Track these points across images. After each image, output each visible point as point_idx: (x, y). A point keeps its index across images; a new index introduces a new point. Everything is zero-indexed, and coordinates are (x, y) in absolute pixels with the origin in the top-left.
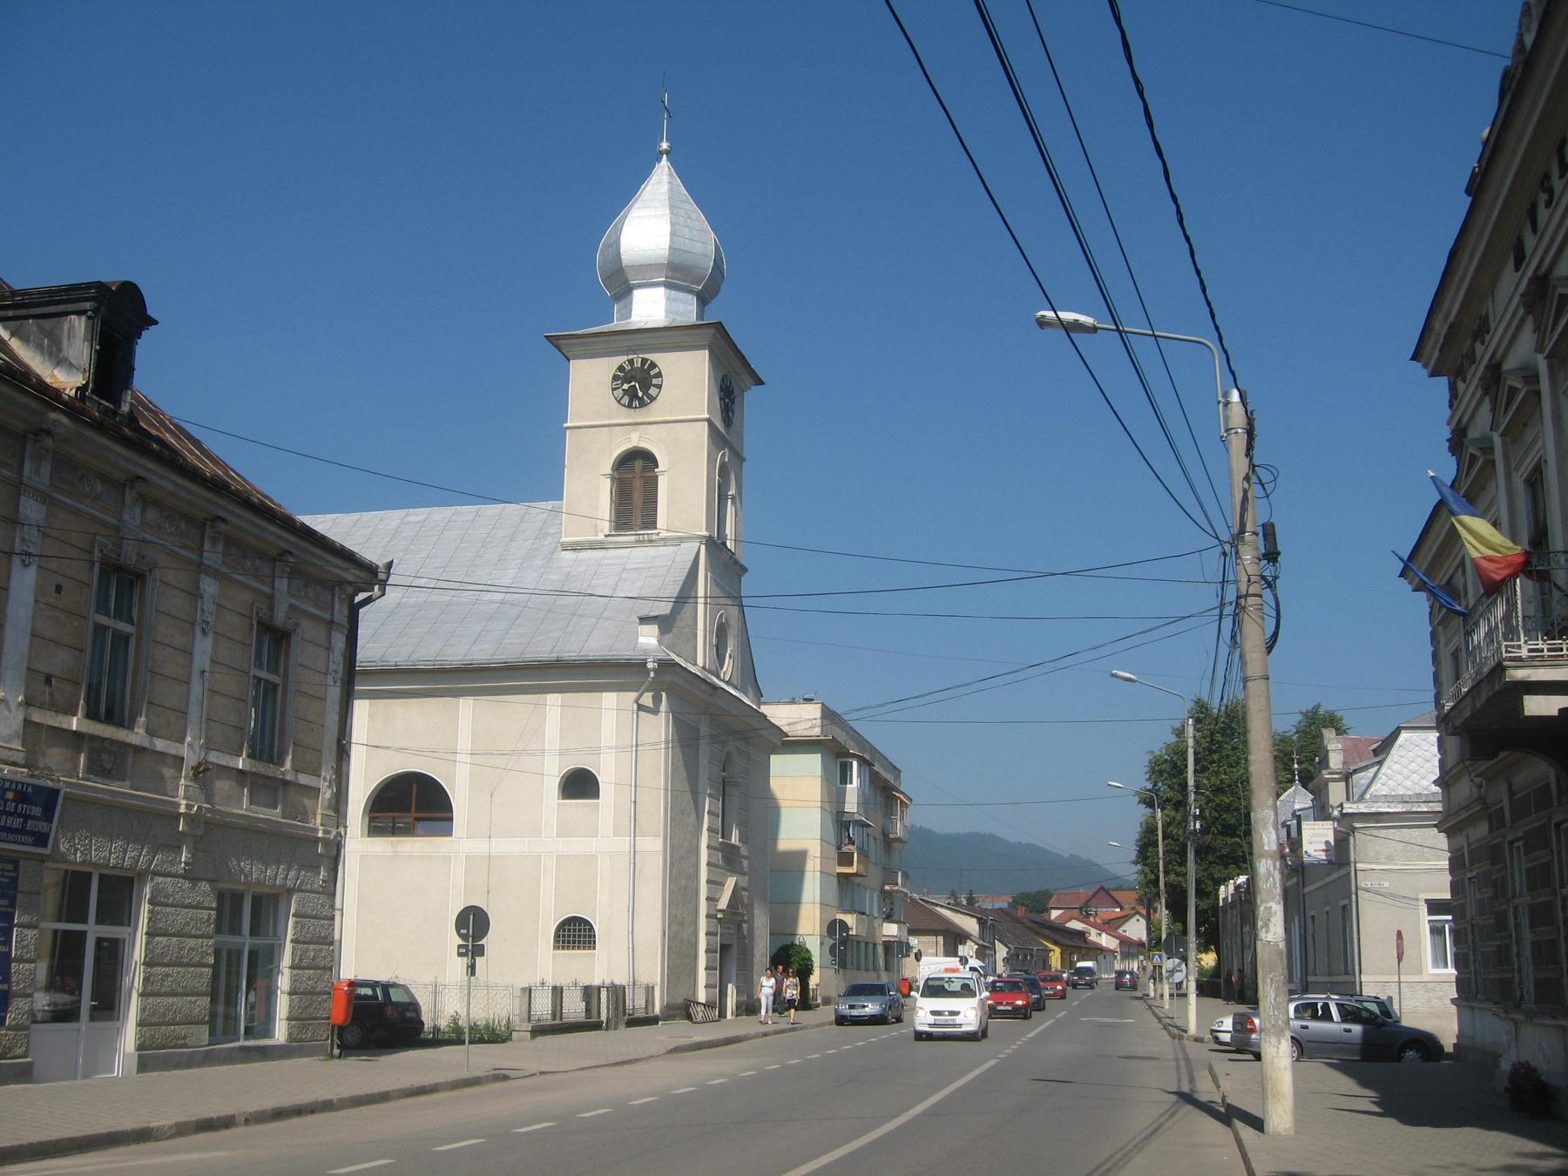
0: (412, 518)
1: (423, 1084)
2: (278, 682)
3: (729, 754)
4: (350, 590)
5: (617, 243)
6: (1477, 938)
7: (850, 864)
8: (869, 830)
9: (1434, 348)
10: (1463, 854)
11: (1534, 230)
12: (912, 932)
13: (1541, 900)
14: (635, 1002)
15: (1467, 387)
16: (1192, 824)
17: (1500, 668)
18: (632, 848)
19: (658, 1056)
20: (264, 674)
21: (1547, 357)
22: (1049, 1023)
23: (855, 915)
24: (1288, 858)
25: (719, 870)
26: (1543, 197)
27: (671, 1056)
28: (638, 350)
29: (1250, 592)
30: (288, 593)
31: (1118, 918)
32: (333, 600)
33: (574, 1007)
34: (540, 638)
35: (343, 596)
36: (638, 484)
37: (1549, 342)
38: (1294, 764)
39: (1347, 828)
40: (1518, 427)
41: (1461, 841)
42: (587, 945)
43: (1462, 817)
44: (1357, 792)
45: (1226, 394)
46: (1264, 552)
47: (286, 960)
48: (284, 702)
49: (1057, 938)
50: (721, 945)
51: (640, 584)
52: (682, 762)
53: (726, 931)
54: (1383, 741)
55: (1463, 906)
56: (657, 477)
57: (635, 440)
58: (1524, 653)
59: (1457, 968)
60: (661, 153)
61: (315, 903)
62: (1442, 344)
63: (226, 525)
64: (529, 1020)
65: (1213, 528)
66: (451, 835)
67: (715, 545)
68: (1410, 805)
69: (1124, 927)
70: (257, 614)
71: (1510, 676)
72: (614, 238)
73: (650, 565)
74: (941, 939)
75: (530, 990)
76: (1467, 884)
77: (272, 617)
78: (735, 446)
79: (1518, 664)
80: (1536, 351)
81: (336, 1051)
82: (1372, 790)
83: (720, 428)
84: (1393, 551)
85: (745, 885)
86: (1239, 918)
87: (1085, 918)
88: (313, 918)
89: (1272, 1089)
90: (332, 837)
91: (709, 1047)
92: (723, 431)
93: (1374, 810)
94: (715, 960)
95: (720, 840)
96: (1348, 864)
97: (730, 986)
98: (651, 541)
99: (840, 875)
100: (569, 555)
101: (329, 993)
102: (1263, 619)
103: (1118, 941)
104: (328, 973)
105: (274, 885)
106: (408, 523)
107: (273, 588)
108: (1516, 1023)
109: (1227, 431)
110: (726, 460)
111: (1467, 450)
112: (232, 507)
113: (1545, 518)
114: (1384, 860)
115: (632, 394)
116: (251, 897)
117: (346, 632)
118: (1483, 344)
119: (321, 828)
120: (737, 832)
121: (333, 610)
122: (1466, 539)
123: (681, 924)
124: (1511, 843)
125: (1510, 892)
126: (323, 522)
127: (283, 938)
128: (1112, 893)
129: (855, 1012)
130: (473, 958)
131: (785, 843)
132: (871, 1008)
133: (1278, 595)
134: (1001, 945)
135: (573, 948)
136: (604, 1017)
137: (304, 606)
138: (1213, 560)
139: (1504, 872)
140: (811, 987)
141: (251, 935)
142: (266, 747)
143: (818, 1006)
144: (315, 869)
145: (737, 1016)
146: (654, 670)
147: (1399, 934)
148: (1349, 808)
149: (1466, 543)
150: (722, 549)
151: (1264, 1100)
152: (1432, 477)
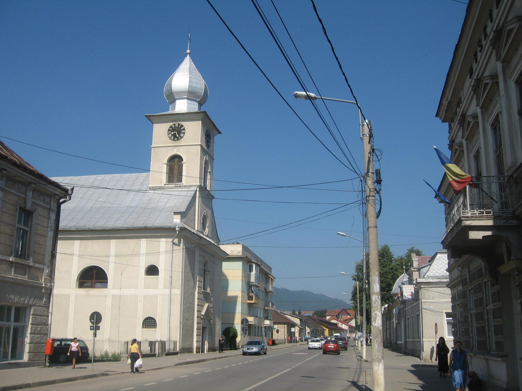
0: (98, 178)
1: (71, 377)
2: (28, 230)
3: (206, 261)
4: (57, 197)
5: (171, 84)
6: (460, 325)
7: (252, 300)
8: (259, 288)
9: (443, 111)
10: (456, 296)
12: (275, 323)
13: (479, 311)
14: (169, 347)
17: (460, 221)
18: (170, 293)
19: (171, 366)
21: (480, 108)
22: (317, 355)
23: (253, 317)
24: (400, 298)
25: (202, 301)
26: (479, 49)
27: (176, 366)
29: (370, 195)
30: (33, 197)
31: (349, 319)
34: (139, 219)
35: (55, 200)
36: (176, 167)
37: (481, 102)
38: (403, 266)
39: (418, 287)
40: (470, 137)
41: (455, 291)
42: (154, 327)
44: (422, 275)
46: (376, 180)
47: (29, 331)
48: (30, 237)
49: (327, 325)
50: (202, 327)
51: (175, 201)
52: (188, 263)
53: (205, 322)
54: (432, 258)
55: (456, 314)
56: (183, 164)
57: (175, 152)
58: (469, 215)
60: (187, 54)
62: (446, 110)
63: (6, 171)
65: (354, 169)
67: (203, 188)
68: (440, 279)
69: (350, 322)
70: (19, 205)
74: (286, 326)
75: (128, 343)
76: (457, 306)
77: (25, 206)
78: (211, 154)
79: (467, 219)
80: (476, 106)
81: (47, 364)
82: (427, 274)
84: (423, 180)
85: (212, 306)
90: (48, 286)
91: (192, 363)
92: (206, 149)
93: (427, 281)
95: (203, 291)
96: (419, 300)
97: (206, 341)
98: (180, 186)
99: (248, 303)
101: (46, 343)
102: (375, 205)
103: (348, 327)
104: (46, 336)
105: (24, 304)
107: (26, 196)
109: (363, 135)
111: (454, 148)
112: (8, 165)
113: (481, 170)
114: (431, 299)
116: (14, 308)
117: (56, 212)
118: (459, 108)
119: (44, 283)
121: (50, 205)
122: (447, 173)
124: (470, 290)
125: (469, 308)
126: (68, 179)
128: (347, 311)
129: (249, 351)
130: (96, 330)
132: (255, 349)
133: (381, 196)
135: (149, 328)
136: (157, 352)
139: (467, 302)
140: (237, 342)
141: (14, 322)
142: (23, 255)
143: (240, 348)
144: (41, 298)
145: (208, 352)
146: (178, 231)
147: (436, 325)
148: (419, 280)
149: (448, 175)
151: (373, 388)
152: (435, 148)
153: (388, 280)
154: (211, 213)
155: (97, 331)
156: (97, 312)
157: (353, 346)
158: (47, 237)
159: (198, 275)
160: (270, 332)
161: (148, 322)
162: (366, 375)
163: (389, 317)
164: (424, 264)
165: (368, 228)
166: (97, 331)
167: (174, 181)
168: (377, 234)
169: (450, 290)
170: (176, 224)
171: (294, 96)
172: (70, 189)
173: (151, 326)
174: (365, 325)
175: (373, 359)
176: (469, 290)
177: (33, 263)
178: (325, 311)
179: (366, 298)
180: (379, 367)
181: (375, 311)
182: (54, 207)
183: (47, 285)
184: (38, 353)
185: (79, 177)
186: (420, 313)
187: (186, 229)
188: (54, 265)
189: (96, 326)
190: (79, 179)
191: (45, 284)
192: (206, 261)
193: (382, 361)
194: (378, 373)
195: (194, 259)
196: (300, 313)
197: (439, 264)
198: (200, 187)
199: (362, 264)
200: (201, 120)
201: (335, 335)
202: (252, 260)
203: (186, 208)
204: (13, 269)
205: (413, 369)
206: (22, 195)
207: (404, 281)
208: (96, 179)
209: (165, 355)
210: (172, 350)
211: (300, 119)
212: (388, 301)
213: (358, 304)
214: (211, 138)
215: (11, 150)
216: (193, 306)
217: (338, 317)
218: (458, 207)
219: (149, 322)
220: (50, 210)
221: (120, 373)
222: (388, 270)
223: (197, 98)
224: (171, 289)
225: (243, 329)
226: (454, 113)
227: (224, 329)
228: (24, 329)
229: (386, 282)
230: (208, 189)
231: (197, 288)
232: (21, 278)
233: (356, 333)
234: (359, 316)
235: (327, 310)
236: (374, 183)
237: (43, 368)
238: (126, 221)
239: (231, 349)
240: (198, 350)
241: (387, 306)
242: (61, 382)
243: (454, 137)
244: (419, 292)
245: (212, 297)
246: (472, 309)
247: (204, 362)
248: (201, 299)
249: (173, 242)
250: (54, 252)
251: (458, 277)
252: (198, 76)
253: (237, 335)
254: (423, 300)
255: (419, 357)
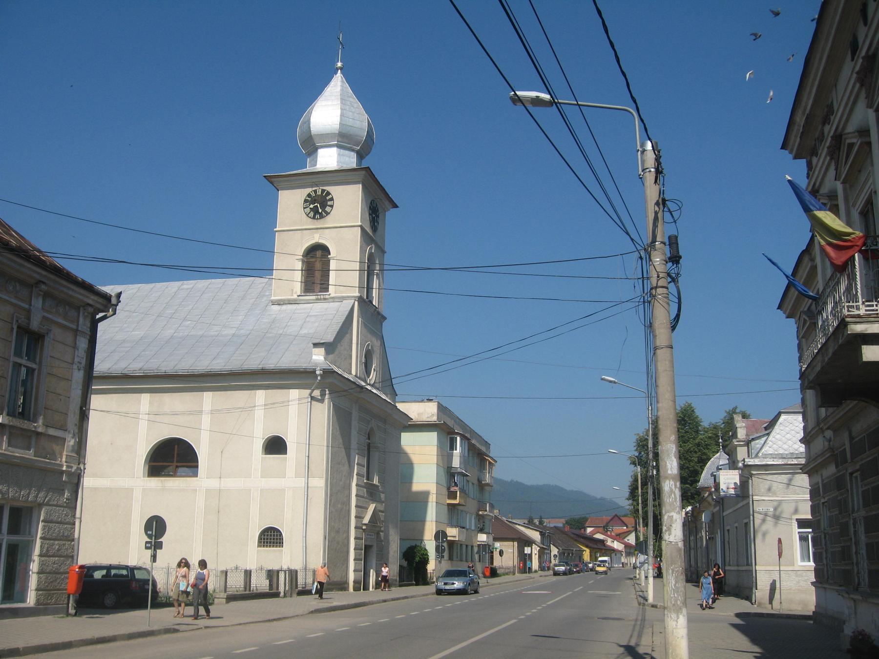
0: (185, 286)
3: (372, 430)
6: (828, 542)
7: (456, 498)
9: (796, 136)
10: (819, 487)
11: (865, 24)
12: (496, 539)
15: (819, 158)
16: (651, 471)
17: (843, 324)
18: (306, 484)
19: (302, 615)
20: (24, 361)
27: (310, 615)
28: (319, 184)
29: (659, 285)
30: (43, 309)
31: (625, 532)
32: (79, 316)
33: (260, 583)
35: (86, 314)
36: (318, 265)
39: (747, 472)
41: (817, 478)
42: (265, 544)
43: (818, 462)
44: (754, 452)
45: (643, 145)
47: (37, 551)
50: (365, 545)
51: (317, 324)
52: (339, 432)
53: (369, 537)
54: (770, 422)
55: (819, 521)
58: (862, 312)
59: (815, 561)
60: (337, 69)
61: (59, 513)
64: (225, 591)
66: (197, 477)
67: (365, 302)
69: (628, 538)
70: (17, 321)
71: (851, 330)
72: (307, 119)
73: (323, 313)
74: (516, 544)
75: (226, 572)
77: (29, 324)
79: (858, 320)
81: (72, 611)
83: (369, 231)
85: (382, 509)
86: (688, 531)
87: (604, 533)
88: (57, 523)
89: (672, 653)
90: (73, 471)
92: (371, 234)
93: (764, 463)
94: (361, 554)
95: (365, 481)
96: (748, 497)
97: (372, 570)
98: (325, 299)
99: (449, 505)
100: (276, 308)
103: (624, 545)
105: (27, 501)
106: (182, 289)
107: (30, 305)
108: (855, 601)
110: (373, 251)
115: (315, 210)
116: (9, 508)
117: (88, 337)
119: (65, 464)
120: (377, 478)
123: (338, 532)
124: (851, 474)
126: (132, 289)
127: (35, 536)
129: (447, 587)
130: (155, 550)
131: (416, 487)
132: (458, 584)
134: (554, 547)
135: (270, 546)
136: (281, 589)
137: (55, 319)
138: (633, 264)
140: (429, 571)
141: (8, 534)
143: (434, 583)
145: (376, 588)
146: (321, 375)
147: (780, 541)
150: (369, 305)
152: (789, 181)
153: (692, 464)
154: (381, 345)
155: (158, 551)
156: (161, 517)
157: (631, 579)
158: (71, 381)
159: (358, 454)
160: (486, 553)
161: (267, 535)
162: (653, 634)
163: (695, 529)
164: (757, 433)
165: (656, 349)
166: (158, 550)
167: (315, 290)
168: (672, 362)
169: (808, 477)
170: (316, 365)
171: (510, 100)
172: (115, 295)
173: (274, 543)
174: (651, 542)
175: (666, 606)
176: (849, 473)
177: (45, 427)
178: (583, 518)
179: (654, 493)
180: (677, 622)
181: (668, 512)
182: (85, 328)
183: (71, 467)
184: (55, 590)
185: (151, 286)
186: (750, 521)
187: (335, 371)
188: (84, 429)
189: (155, 542)
190: (152, 289)
191: (67, 466)
192: (372, 430)
193: (684, 611)
194: (675, 634)
195: (350, 425)
196: (541, 522)
197: (783, 433)
198: (360, 299)
199: (646, 437)
200: (361, 183)
201: (600, 559)
202: (455, 428)
203: (335, 335)
204: (5, 437)
205: (738, 621)
206: (22, 304)
207: (720, 464)
208: (181, 287)
209: (296, 594)
210: (241, 589)
211: (491, 62)
212: (693, 501)
213: (640, 505)
214: (380, 215)
215: (7, 225)
216: (347, 509)
217: (607, 529)
218: (836, 303)
219: (271, 535)
220: (76, 332)
221: (202, 628)
222: (692, 447)
223: (355, 146)
224: (308, 478)
225: (438, 549)
226: (818, 139)
227: (405, 550)
228: (28, 546)
229: (690, 468)
230: (374, 303)
231: (355, 476)
232: (21, 455)
233: (637, 556)
234: (641, 526)
235: (587, 516)
236: (667, 263)
237: (63, 617)
238: (230, 360)
239: (417, 584)
240: (357, 585)
241: (691, 509)
242: (82, 646)
243: (818, 183)
244: (748, 482)
245: (383, 493)
246: (856, 510)
247: (365, 607)
248: (363, 497)
249: (312, 395)
250: (84, 409)
251: (824, 452)
252: (355, 106)
253: (428, 559)
254: (755, 498)
255: (748, 598)
